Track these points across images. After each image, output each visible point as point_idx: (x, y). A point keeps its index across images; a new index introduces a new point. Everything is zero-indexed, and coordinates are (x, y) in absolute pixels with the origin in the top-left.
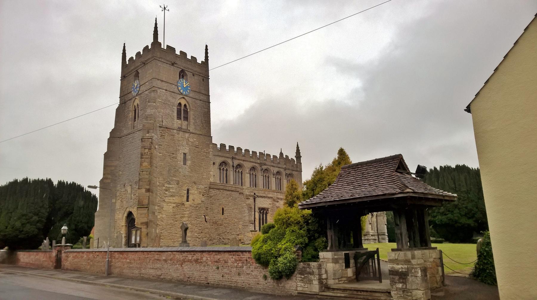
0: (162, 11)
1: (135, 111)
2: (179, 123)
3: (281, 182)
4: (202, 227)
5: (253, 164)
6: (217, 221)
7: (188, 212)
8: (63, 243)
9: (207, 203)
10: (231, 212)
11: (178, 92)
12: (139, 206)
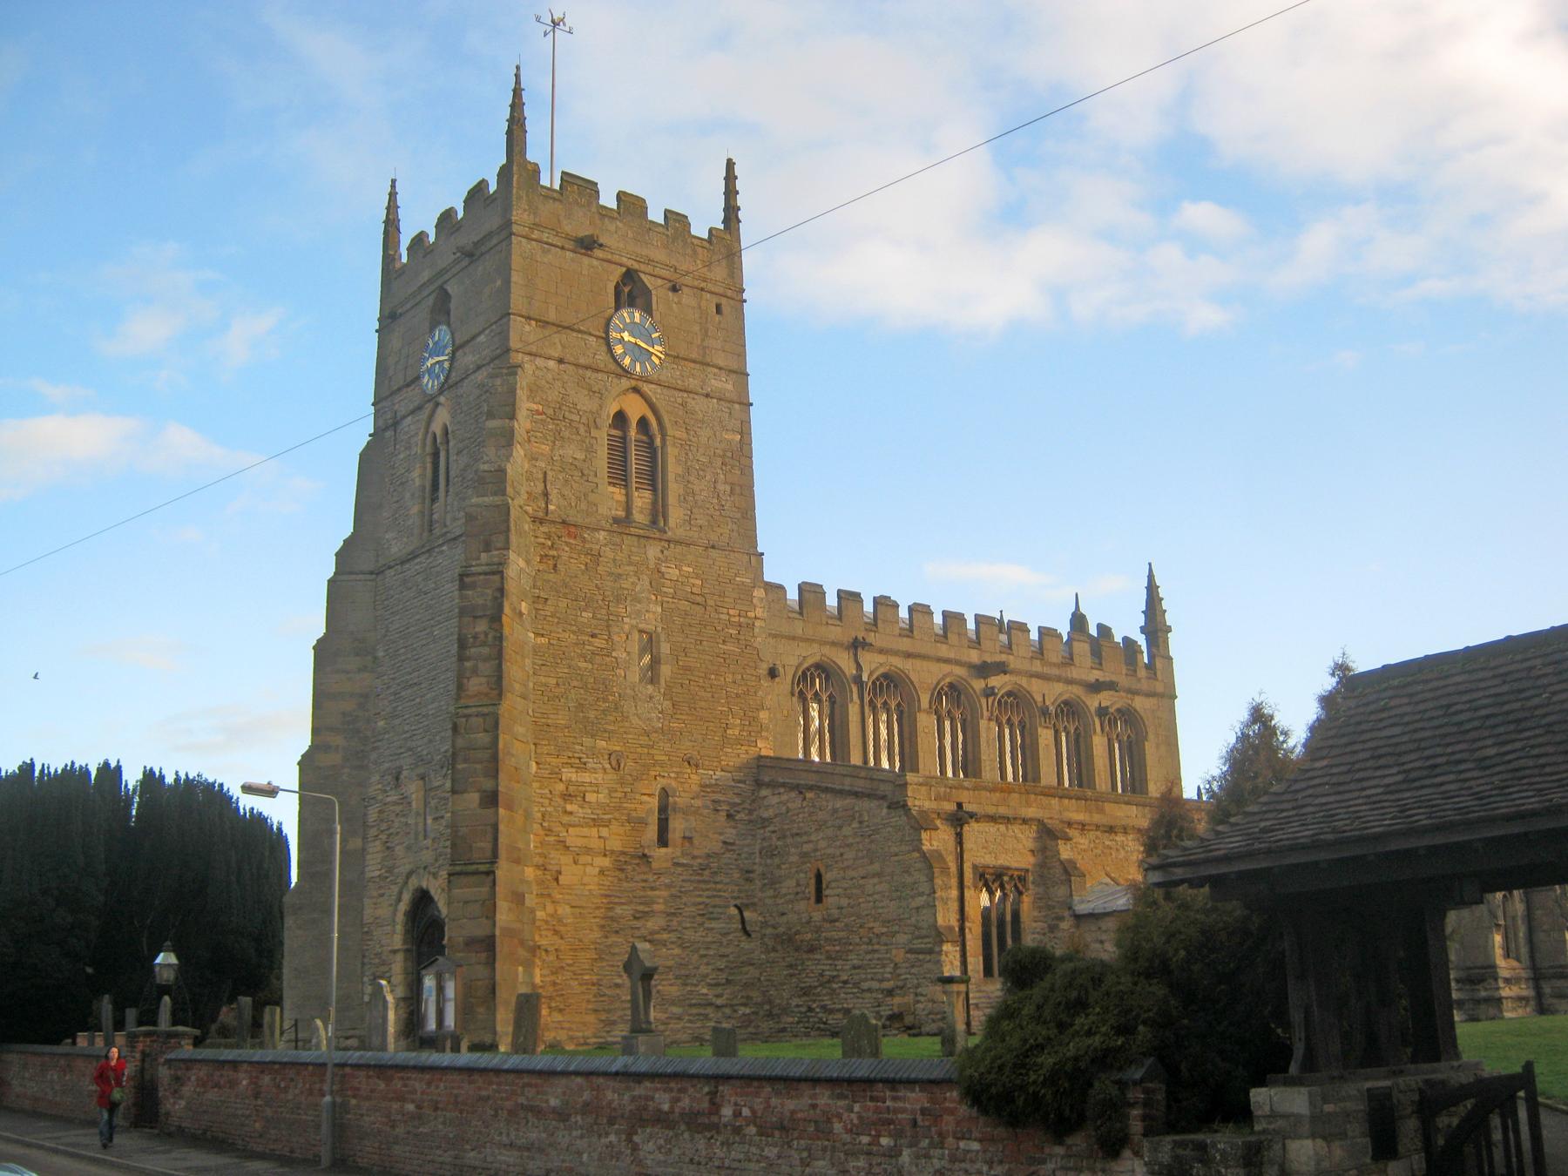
0: (545, 34)
1: (436, 455)
5: (947, 668)
6: (793, 930)
7: (665, 893)
8: (164, 1023)
9: (746, 849)
10: (854, 891)
11: (612, 366)
12: (458, 868)
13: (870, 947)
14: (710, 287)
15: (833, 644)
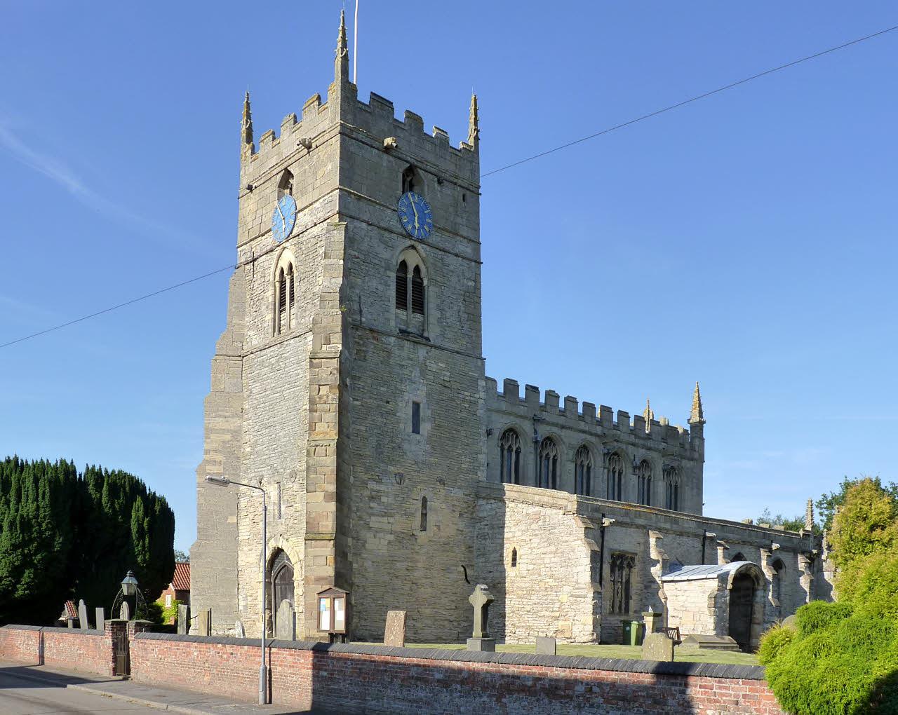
2: (402, 319)
3: (651, 487)
4: (458, 595)
5: (583, 436)
6: (497, 581)
13: (545, 593)
14: (460, 182)
15: (521, 417)
